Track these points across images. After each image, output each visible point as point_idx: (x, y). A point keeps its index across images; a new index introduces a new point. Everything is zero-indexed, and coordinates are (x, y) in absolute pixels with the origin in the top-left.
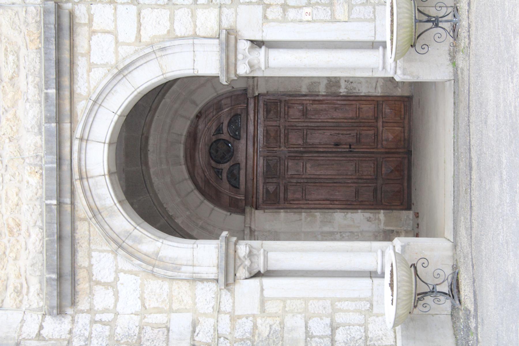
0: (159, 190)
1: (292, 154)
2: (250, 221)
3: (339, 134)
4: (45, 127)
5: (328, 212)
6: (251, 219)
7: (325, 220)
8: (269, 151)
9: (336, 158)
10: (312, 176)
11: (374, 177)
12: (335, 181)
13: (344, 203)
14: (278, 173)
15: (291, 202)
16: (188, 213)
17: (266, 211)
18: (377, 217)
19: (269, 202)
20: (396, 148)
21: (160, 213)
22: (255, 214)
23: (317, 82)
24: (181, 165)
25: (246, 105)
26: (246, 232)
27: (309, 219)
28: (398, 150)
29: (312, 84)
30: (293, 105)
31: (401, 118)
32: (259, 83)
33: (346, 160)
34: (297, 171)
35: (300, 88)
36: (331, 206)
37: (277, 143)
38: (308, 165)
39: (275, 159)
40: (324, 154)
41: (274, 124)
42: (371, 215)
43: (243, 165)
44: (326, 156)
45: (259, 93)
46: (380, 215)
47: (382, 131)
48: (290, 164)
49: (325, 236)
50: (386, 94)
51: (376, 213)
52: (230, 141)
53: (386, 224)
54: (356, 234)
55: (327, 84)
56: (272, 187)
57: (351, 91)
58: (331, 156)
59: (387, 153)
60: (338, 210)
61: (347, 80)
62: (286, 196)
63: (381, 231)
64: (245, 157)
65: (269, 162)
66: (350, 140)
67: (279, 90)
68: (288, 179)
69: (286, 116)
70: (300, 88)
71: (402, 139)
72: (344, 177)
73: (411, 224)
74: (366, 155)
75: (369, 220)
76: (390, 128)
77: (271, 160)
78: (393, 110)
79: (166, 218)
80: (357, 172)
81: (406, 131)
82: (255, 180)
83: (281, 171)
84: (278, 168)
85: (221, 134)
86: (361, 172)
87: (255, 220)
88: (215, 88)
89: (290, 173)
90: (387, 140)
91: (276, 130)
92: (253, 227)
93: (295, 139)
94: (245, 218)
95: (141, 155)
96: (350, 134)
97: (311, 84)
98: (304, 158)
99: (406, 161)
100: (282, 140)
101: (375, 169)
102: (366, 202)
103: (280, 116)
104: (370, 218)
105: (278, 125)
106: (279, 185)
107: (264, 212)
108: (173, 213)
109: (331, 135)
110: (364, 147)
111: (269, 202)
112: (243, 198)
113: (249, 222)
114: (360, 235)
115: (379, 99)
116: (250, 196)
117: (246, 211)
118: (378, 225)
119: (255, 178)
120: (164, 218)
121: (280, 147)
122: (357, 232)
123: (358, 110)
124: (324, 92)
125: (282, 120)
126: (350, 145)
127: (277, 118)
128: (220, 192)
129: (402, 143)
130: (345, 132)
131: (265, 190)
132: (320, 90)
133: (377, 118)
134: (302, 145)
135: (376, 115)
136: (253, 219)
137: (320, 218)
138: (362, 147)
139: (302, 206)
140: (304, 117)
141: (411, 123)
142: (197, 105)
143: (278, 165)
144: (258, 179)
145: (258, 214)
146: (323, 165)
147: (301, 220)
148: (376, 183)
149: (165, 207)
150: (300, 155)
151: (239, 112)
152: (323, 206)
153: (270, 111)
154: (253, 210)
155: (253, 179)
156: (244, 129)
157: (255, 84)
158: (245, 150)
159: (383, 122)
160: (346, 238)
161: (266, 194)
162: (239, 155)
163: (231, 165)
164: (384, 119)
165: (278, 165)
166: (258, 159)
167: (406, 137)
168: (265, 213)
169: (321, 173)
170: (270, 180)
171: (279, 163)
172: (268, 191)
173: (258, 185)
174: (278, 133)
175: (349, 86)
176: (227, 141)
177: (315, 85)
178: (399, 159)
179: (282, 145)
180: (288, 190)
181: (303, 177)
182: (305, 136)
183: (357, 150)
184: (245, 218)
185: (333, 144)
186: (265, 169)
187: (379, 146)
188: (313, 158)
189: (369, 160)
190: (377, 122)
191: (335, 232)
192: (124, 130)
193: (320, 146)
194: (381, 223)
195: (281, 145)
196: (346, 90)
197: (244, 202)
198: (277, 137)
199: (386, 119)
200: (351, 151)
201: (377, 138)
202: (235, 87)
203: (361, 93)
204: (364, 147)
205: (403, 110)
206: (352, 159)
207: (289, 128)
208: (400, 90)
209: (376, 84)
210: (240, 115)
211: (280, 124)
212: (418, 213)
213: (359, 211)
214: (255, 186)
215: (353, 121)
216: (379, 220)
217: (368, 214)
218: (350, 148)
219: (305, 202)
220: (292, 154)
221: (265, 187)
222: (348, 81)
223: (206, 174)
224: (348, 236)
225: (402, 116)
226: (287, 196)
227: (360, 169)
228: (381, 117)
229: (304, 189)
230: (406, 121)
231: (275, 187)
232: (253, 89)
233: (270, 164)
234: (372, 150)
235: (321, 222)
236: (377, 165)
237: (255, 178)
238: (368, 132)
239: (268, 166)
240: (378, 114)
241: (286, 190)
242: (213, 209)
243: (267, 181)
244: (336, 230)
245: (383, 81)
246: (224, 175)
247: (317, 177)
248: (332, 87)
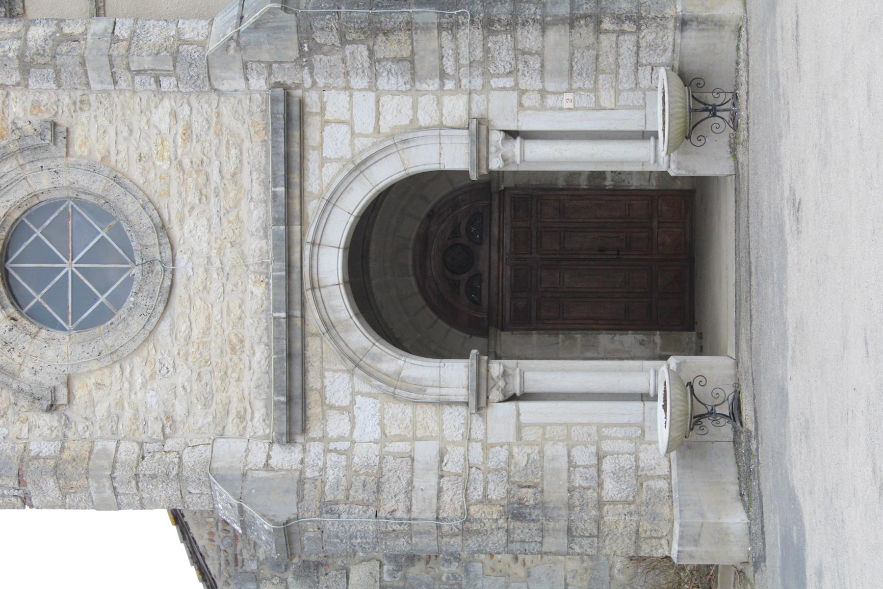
6: (496, 342)
17: (514, 332)
18: (652, 339)
27: (567, 342)
36: (594, 326)
42: (645, 338)
46: (655, 337)
50: (663, 188)
60: (604, 332)
75: (642, 343)
82: (500, 294)
96: (617, 237)
104: (643, 340)
107: (512, 334)
109: (594, 238)
121: (531, 253)
126: (618, 251)
136: (498, 343)
137: (581, 341)
154: (499, 331)
155: (499, 293)
196: (612, 183)
213: (630, 332)
216: (655, 344)
232: (498, 182)
234: (645, 257)
246: (462, 289)
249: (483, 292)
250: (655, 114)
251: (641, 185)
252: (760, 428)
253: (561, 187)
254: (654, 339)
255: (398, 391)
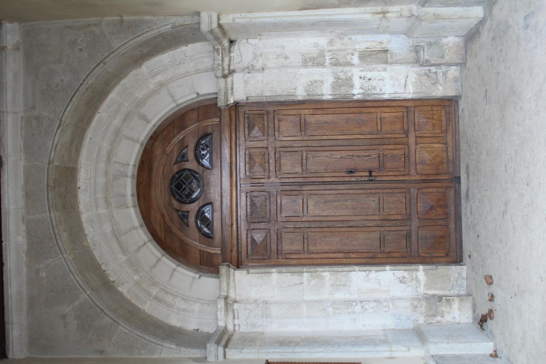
0: (94, 245)
1: (288, 188)
2: (228, 288)
3: (353, 156)
4: (179, 182)
5: (342, 271)
6: (228, 284)
7: (338, 283)
8: (253, 185)
9: (350, 191)
10: (317, 219)
11: (405, 217)
12: (350, 224)
13: (364, 255)
15: (288, 256)
16: (136, 277)
17: (251, 271)
18: (414, 276)
21: (80, 285)
22: (234, 276)
23: (319, 81)
25: (218, 120)
26: (219, 306)
27: (313, 282)
28: (439, 177)
29: (312, 83)
30: (286, 117)
31: (442, 131)
32: (235, 86)
33: (365, 194)
34: (295, 211)
35: (294, 91)
36: (345, 261)
37: (265, 171)
38: (311, 203)
39: (263, 195)
41: (260, 144)
42: (406, 274)
43: (217, 204)
45: (235, 99)
46: (418, 273)
48: (284, 202)
49: (338, 309)
50: (421, 95)
52: (198, 171)
53: (427, 286)
54: (384, 304)
55: (334, 82)
56: (259, 235)
57: (369, 92)
58: (343, 188)
59: (424, 181)
60: (357, 268)
61: (362, 76)
62: (280, 248)
63: (420, 297)
64: (220, 194)
65: (253, 199)
66: (369, 165)
67: (264, 95)
68: (282, 224)
69: (276, 133)
70: (294, 91)
71: (445, 160)
72: (363, 218)
73: (465, 285)
74: (394, 185)
75: (402, 281)
76: (427, 145)
77: (257, 197)
78: (430, 119)
79: (88, 292)
80: (381, 210)
82: (235, 226)
83: (272, 213)
84: (268, 208)
85: (185, 161)
86: (387, 211)
88: (172, 96)
89: (284, 215)
91: (263, 153)
92: (232, 295)
94: (220, 281)
95: (48, 195)
96: (369, 156)
97: (310, 83)
99: (451, 193)
100: (272, 168)
101: (408, 205)
103: (268, 134)
104: (404, 278)
105: (265, 146)
106: (270, 232)
107: (248, 273)
108: (115, 278)
109: (341, 157)
110: (390, 173)
112: (219, 252)
114: (391, 306)
115: (408, 104)
116: (229, 250)
117: (220, 272)
118: (416, 287)
120: (86, 292)
121: (269, 178)
122: (386, 301)
123: (379, 121)
125: (271, 139)
126: (370, 172)
127: (264, 136)
128: (187, 244)
129: (445, 166)
130: (362, 153)
131: (249, 240)
132: (324, 92)
133: (408, 130)
136: (232, 284)
137: (330, 279)
138: (387, 174)
139: (304, 261)
140: (303, 133)
141: (457, 136)
142: (148, 122)
143: (268, 204)
144: (239, 225)
146: (332, 201)
147: (302, 283)
148: (410, 226)
149: (104, 269)
150: (298, 188)
151: (210, 130)
152: (332, 261)
154: (232, 270)
155: (232, 225)
157: (229, 86)
159: (416, 137)
163: (201, 205)
165: (268, 204)
166: (239, 197)
168: (250, 275)
169: (330, 213)
170: (256, 226)
171: (268, 200)
172: (253, 241)
174: (266, 157)
176: (194, 171)
177: (316, 85)
178: (441, 190)
179: (272, 174)
180: (283, 240)
181: (303, 220)
182: (304, 161)
183: (380, 179)
184: (220, 281)
185: (345, 171)
186: (249, 210)
188: (316, 192)
189: (398, 193)
191: (353, 301)
192: (23, 157)
194: (420, 285)
195: (271, 175)
196: (361, 91)
198: (265, 163)
199: (420, 132)
200: (371, 180)
202: (200, 93)
204: (390, 173)
205: (444, 119)
206: (373, 191)
207: (281, 149)
208: (441, 88)
209: (406, 81)
211: (268, 145)
212: (491, 277)
213: (388, 268)
215: (373, 136)
216: (418, 280)
217: (400, 272)
218: (371, 176)
219: (308, 256)
220: (288, 188)
221: (249, 236)
222: (364, 77)
223: (166, 220)
224: (373, 308)
225: (444, 128)
226: (282, 247)
228: (413, 129)
229: (305, 237)
230: (449, 136)
231: (264, 235)
232: (226, 94)
233: (256, 202)
235: (332, 285)
238: (395, 152)
239: (253, 205)
241: (279, 239)
242: (175, 270)
244: (354, 297)
245: (415, 76)
246: (192, 219)
247: (324, 219)
250: (339, 110)
251: (396, 93)
253: (300, 98)
254: (417, 276)
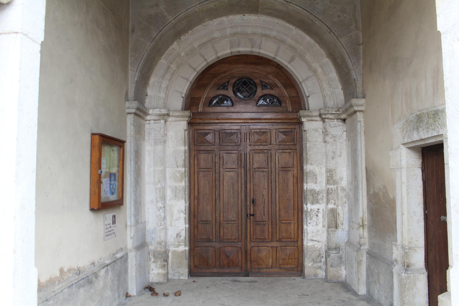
0: (205, 26)
1: (243, 158)
3: (264, 203)
6: (177, 116)
7: (177, 192)
10: (221, 178)
12: (217, 201)
13: (196, 210)
14: (225, 144)
15: (196, 157)
16: (183, 54)
17: (186, 132)
18: (181, 244)
19: (196, 135)
20: (251, 260)
22: (183, 120)
23: (316, 181)
24: (231, 48)
25: (290, 111)
26: (163, 110)
27: (178, 175)
28: (249, 262)
29: (315, 176)
31: (281, 265)
32: (314, 122)
35: (310, 163)
36: (192, 196)
37: (254, 142)
38: (232, 174)
40: (244, 189)
41: (273, 139)
42: (183, 238)
43: (232, 109)
44: (242, 191)
46: (183, 246)
47: (267, 246)
48: (233, 155)
49: (160, 191)
51: (185, 242)
53: (174, 252)
57: (308, 215)
59: (246, 252)
60: (187, 204)
61: (319, 211)
62: (202, 152)
63: (167, 247)
65: (235, 134)
68: (218, 153)
69: (281, 151)
70: (310, 163)
71: (261, 267)
72: (222, 210)
73: (175, 278)
74: (244, 231)
75: (178, 235)
76: (271, 255)
77: (237, 137)
78: (289, 257)
79: (173, 22)
80: (227, 222)
81: (268, 270)
82: (217, 121)
83: (226, 147)
84: (229, 144)
85: (262, 87)
86: (226, 226)
87: (177, 121)
89: (224, 155)
90: (259, 251)
92: (170, 119)
93: (259, 160)
96: (264, 215)
98: (240, 169)
99: (238, 270)
100: (257, 147)
102: (197, 232)
103: (280, 145)
104: (180, 237)
105: (272, 143)
106: (212, 145)
107: (185, 130)
108: (183, 40)
109: (263, 195)
110: (252, 229)
111: (196, 135)
112: (199, 111)
113: (174, 115)
114: (161, 227)
115: (299, 242)
117: (186, 111)
118: (173, 245)
119: (219, 121)
121: (250, 145)
122: (165, 224)
123: (288, 221)
124: (307, 188)
125: (277, 147)
126: (253, 215)
127: (279, 142)
129: (256, 267)
131: (208, 131)
132: (309, 184)
133: (281, 241)
134: (252, 167)
135: (283, 240)
136: (178, 119)
137: (180, 186)
138: (251, 226)
139: (192, 168)
140: (280, 169)
141: (276, 275)
142: (289, 63)
143: (232, 144)
144: (218, 124)
145: (182, 125)
147: (177, 167)
148: (216, 242)
150: (243, 165)
151: (283, 105)
153: (285, 135)
154: (187, 119)
155: (218, 119)
156: (267, 110)
157: (314, 118)
158: (215, 236)
159: (277, 247)
160: (159, 213)
161: (204, 133)
162: (241, 106)
163: (232, 98)
164: (280, 248)
165: (232, 144)
166: (237, 124)
167: (262, 270)
169: (226, 187)
170: (217, 136)
171: (234, 144)
172: (207, 134)
173: (212, 124)
174: (264, 144)
175: (314, 213)
179: (252, 148)
182: (261, 170)
185: (254, 198)
187: (253, 244)
188: (240, 178)
189: (239, 234)
190: (277, 241)
191: (165, 202)
193: (251, 185)
194: (175, 247)
195: (252, 147)
196: (309, 210)
197: (195, 111)
199: (280, 250)
200: (247, 216)
201: (261, 242)
202: (309, 98)
203: (307, 225)
204: (252, 229)
205: (289, 266)
206: (240, 217)
207: (270, 154)
209: (316, 241)
210: (281, 105)
212: (180, 295)
213: (187, 226)
214: (212, 121)
216: (178, 246)
217: (184, 234)
219: (196, 171)
220: (243, 158)
221: (210, 131)
224: (160, 215)
226: (202, 153)
227: (229, 225)
231: (211, 142)
232: (308, 116)
234: (248, 236)
235: (176, 187)
236: (233, 242)
237: (219, 121)
238: (267, 233)
239: (232, 134)
240: (284, 242)
241: (208, 152)
242: (188, 80)
243: (217, 134)
244: (168, 202)
245: (319, 247)
246: (222, 92)
247: (221, 183)
248: (312, 195)
249: (219, 108)
251: (307, 234)
252: (210, 129)
253: (305, 167)
254: (182, 245)
255: (156, 99)
